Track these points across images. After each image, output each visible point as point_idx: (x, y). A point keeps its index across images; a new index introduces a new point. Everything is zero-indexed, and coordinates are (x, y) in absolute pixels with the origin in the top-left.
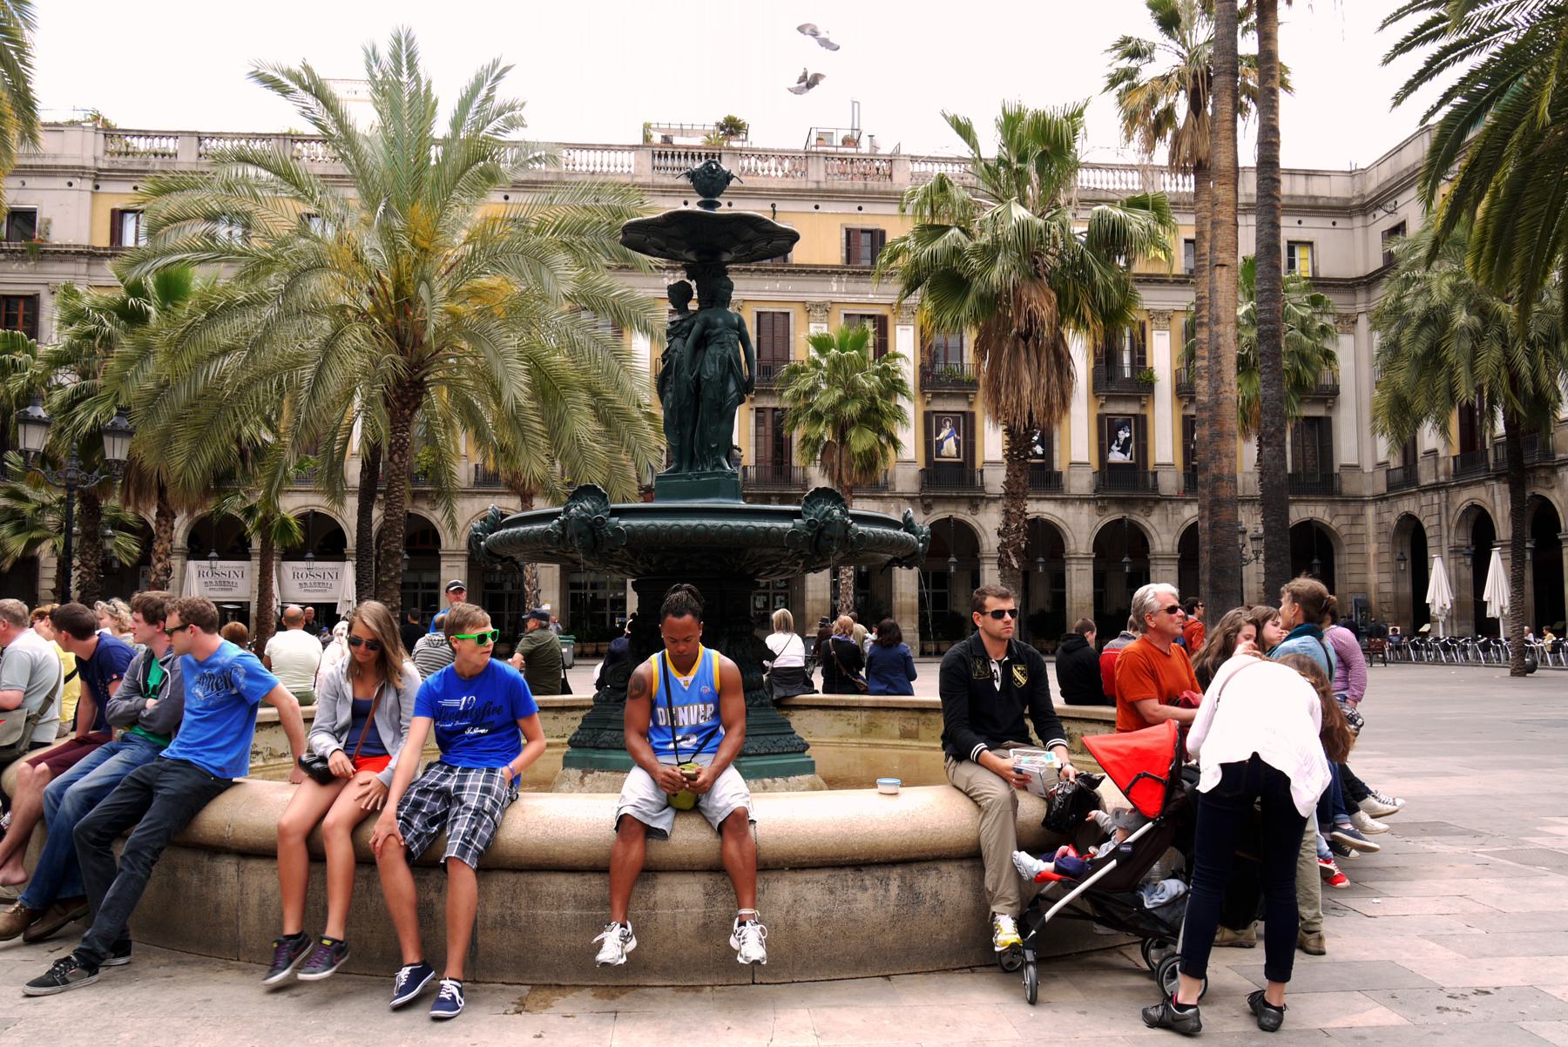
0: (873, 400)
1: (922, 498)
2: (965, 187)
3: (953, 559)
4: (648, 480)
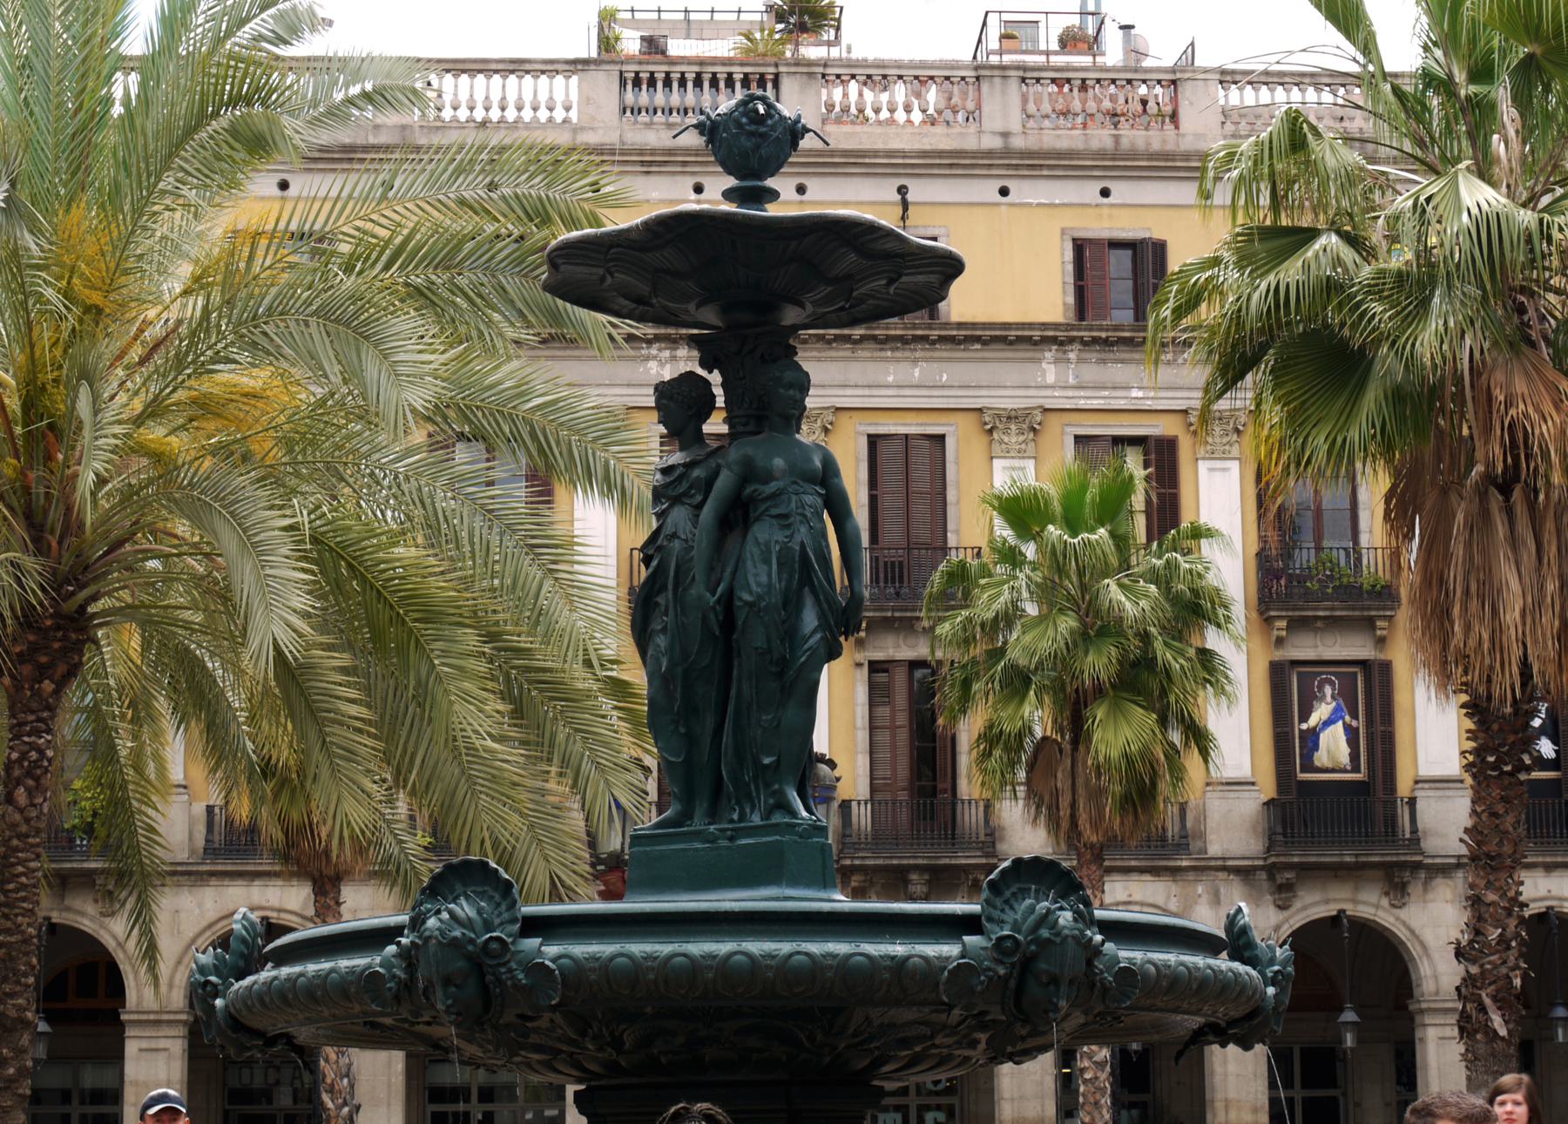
0: (1145, 637)
1: (1271, 870)
2: (1348, 139)
3: (1349, 1016)
4: (613, 842)
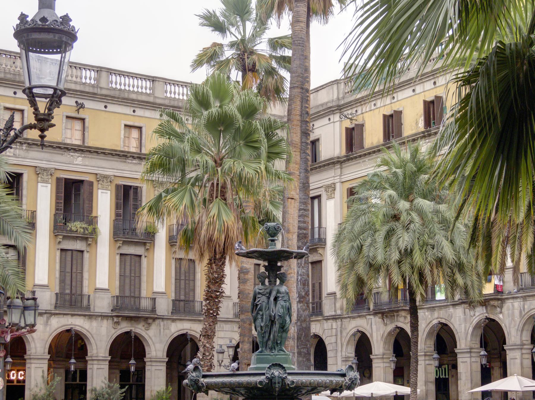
3: (73, 361)
